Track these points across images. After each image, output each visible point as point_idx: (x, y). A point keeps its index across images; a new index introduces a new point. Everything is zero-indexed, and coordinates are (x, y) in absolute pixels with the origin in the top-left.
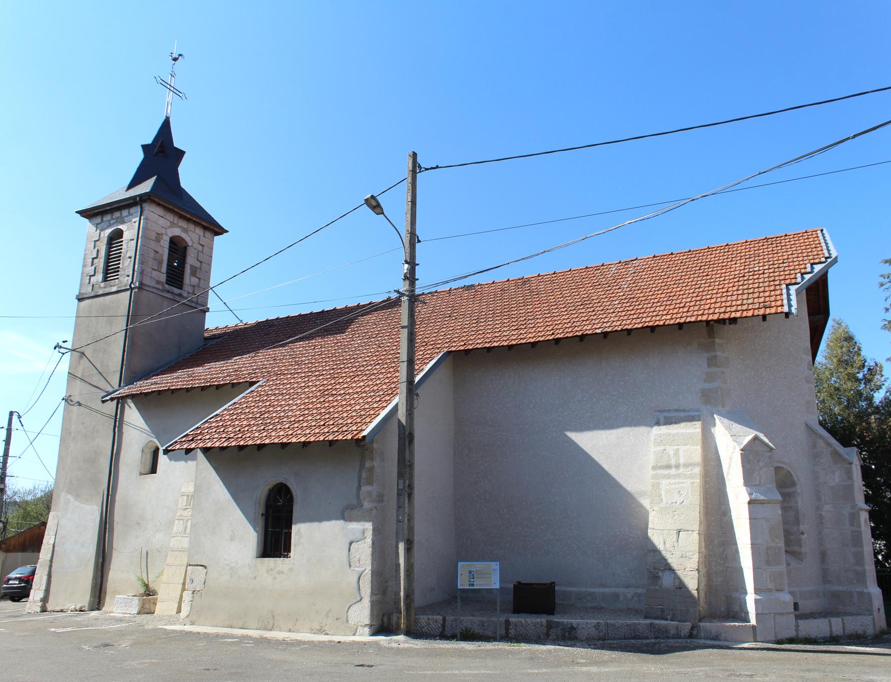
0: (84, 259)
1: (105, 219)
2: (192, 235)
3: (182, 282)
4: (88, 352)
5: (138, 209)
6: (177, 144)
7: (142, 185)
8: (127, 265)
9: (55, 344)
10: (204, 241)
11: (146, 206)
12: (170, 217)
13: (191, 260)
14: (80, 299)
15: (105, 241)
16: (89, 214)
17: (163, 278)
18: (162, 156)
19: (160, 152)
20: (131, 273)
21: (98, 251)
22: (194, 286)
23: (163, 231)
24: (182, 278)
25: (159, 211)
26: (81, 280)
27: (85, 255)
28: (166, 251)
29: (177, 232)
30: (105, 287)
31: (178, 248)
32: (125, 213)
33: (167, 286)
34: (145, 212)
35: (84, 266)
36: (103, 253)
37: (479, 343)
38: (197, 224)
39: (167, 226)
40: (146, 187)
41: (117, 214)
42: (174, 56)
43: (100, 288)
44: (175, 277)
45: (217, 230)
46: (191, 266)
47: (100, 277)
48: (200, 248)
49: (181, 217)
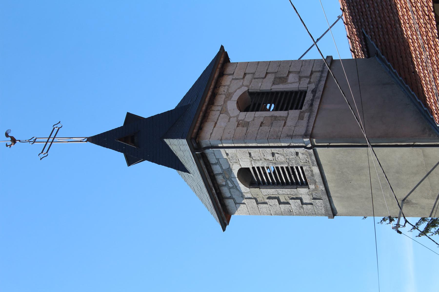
0: (282, 214)
1: (228, 194)
2: (234, 88)
3: (296, 92)
4: (401, 194)
5: (209, 152)
6: (121, 123)
7: (179, 154)
8: (285, 157)
9: (395, 232)
10: (239, 73)
11: (205, 142)
12: (214, 114)
13: (266, 85)
14: (334, 213)
15: (255, 191)
16: (224, 216)
17: (294, 113)
18: (138, 140)
19: (133, 142)
20: (292, 150)
21: (269, 198)
22: (300, 78)
23: (234, 120)
24: (292, 92)
25: (208, 127)
26: (309, 215)
27: (276, 214)
28: (258, 114)
29: (232, 106)
30: (315, 183)
31: (253, 102)
32: (217, 169)
33: (304, 108)
34: (213, 142)
35: (290, 213)
36: (271, 192)
37: (307, 95)
38: (218, 85)
39: (225, 118)
40: (180, 147)
41: (220, 180)
42: (10, 143)
43: (316, 189)
44: (289, 100)
45: (222, 60)
46: (273, 84)
47: (302, 192)
48: (247, 76)
49: (212, 102)
